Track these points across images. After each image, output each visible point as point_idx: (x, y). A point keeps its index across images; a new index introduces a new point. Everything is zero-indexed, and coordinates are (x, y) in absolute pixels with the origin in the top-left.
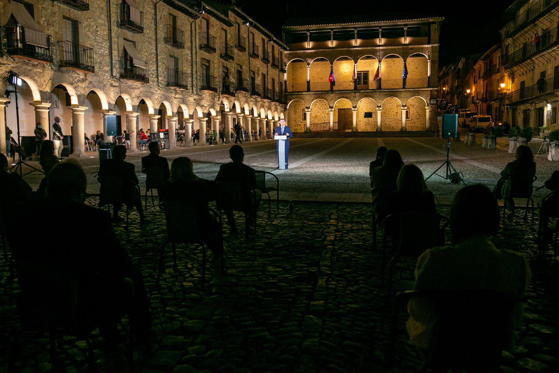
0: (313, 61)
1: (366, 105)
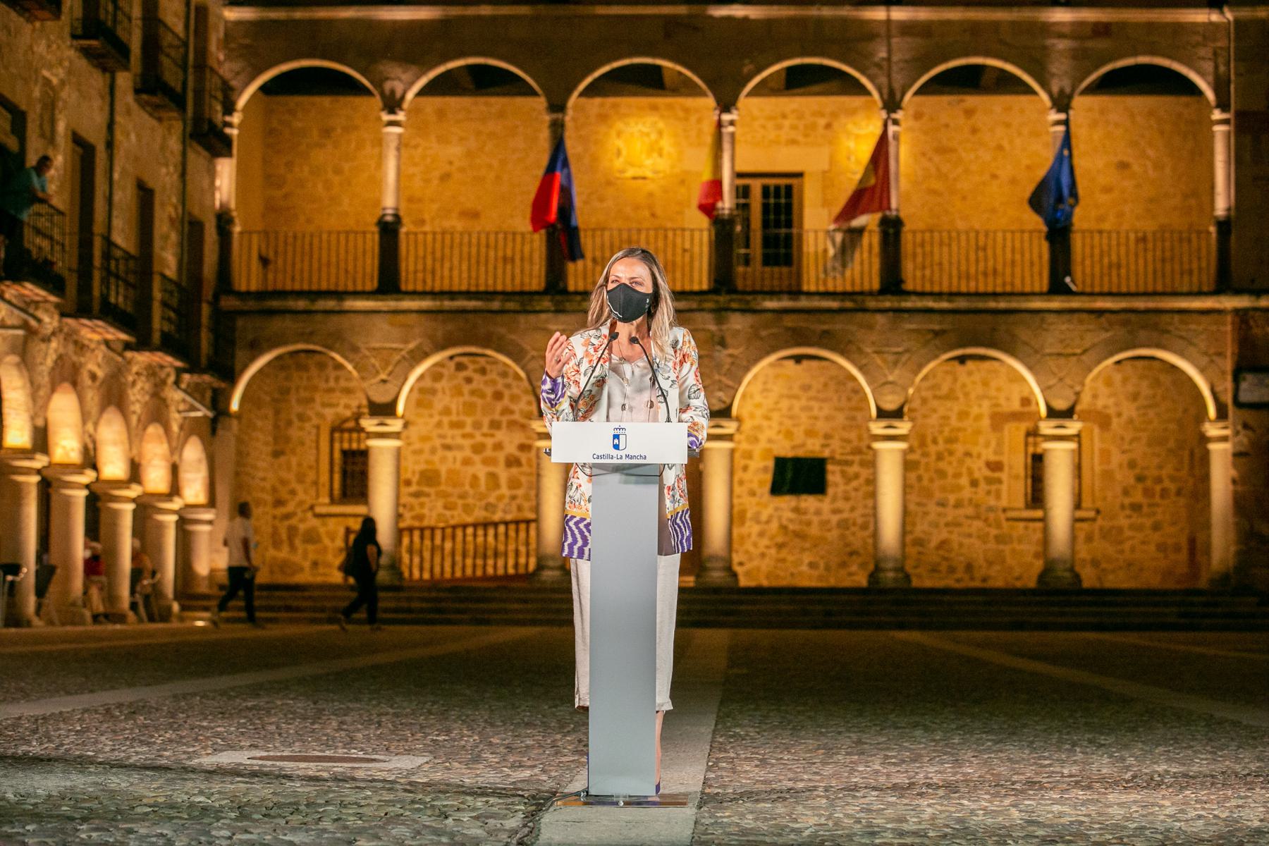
0: (423, 81)
1: (785, 404)
